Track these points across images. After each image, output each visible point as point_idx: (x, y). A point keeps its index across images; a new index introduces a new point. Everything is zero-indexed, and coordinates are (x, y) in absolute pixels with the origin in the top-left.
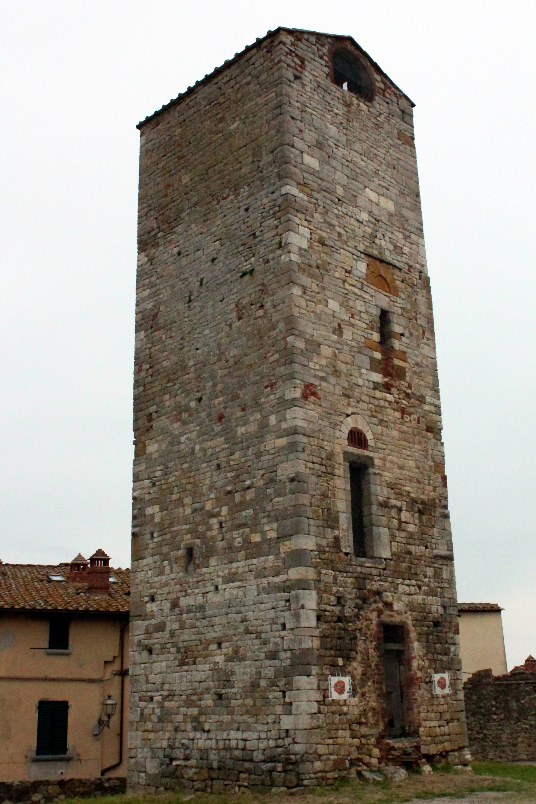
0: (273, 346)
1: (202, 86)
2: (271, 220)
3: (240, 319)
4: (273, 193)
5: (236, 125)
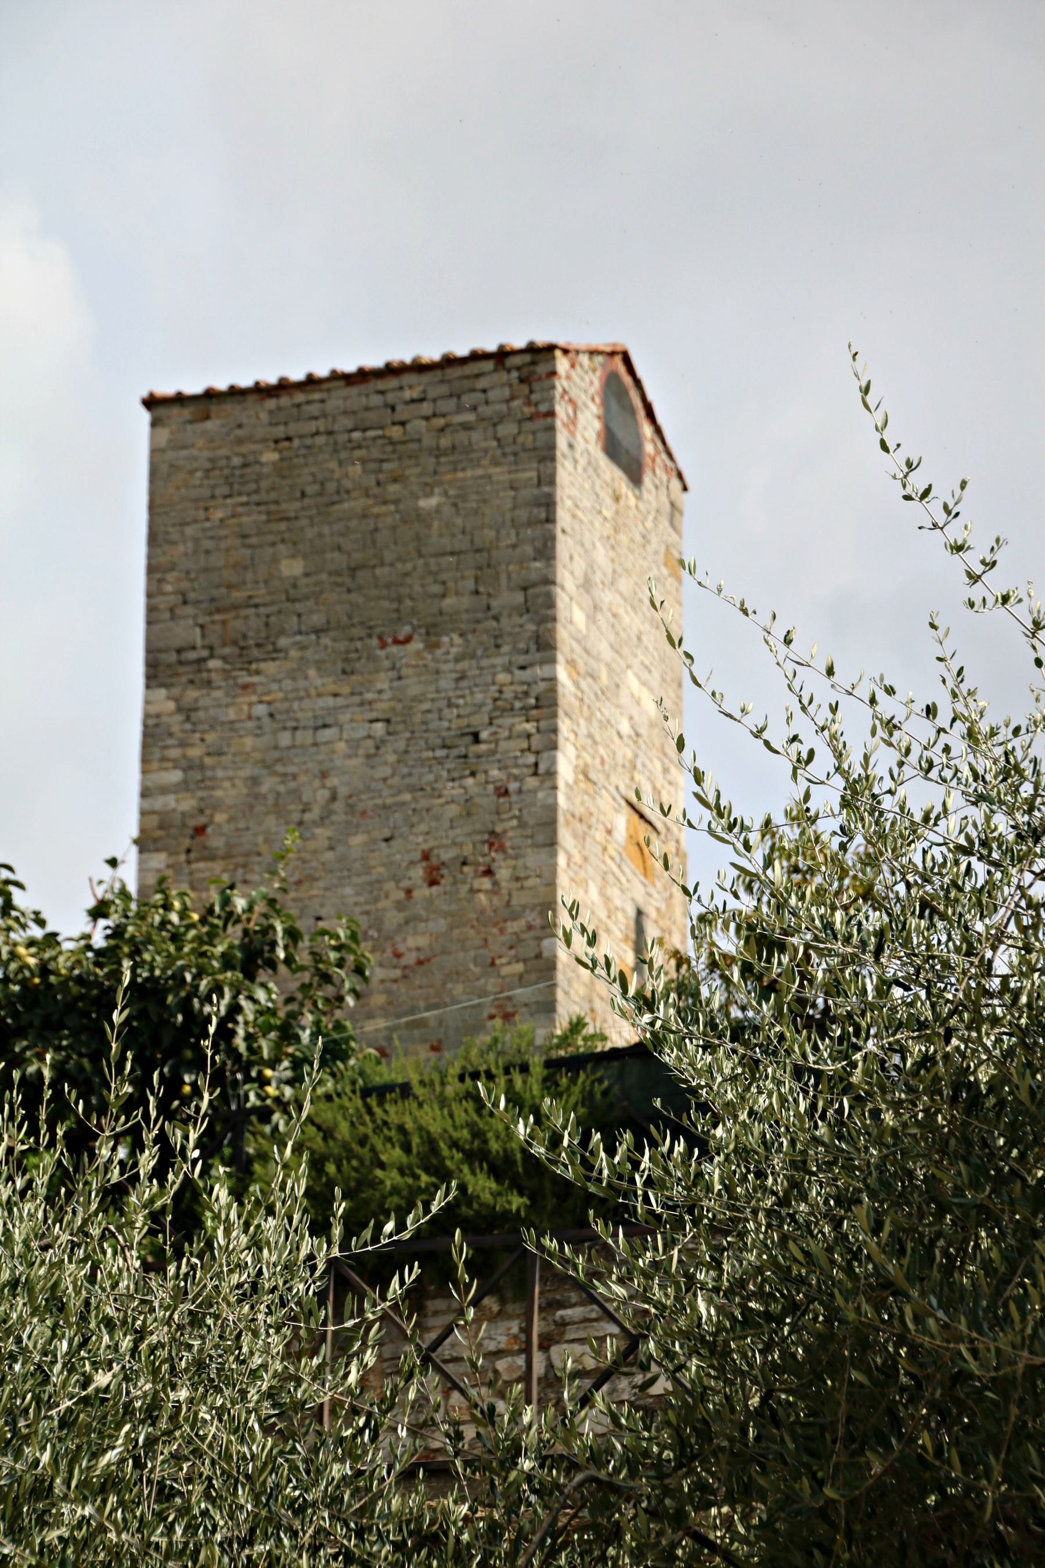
0: (511, 948)
1: (342, 383)
3: (433, 883)
4: (523, 668)
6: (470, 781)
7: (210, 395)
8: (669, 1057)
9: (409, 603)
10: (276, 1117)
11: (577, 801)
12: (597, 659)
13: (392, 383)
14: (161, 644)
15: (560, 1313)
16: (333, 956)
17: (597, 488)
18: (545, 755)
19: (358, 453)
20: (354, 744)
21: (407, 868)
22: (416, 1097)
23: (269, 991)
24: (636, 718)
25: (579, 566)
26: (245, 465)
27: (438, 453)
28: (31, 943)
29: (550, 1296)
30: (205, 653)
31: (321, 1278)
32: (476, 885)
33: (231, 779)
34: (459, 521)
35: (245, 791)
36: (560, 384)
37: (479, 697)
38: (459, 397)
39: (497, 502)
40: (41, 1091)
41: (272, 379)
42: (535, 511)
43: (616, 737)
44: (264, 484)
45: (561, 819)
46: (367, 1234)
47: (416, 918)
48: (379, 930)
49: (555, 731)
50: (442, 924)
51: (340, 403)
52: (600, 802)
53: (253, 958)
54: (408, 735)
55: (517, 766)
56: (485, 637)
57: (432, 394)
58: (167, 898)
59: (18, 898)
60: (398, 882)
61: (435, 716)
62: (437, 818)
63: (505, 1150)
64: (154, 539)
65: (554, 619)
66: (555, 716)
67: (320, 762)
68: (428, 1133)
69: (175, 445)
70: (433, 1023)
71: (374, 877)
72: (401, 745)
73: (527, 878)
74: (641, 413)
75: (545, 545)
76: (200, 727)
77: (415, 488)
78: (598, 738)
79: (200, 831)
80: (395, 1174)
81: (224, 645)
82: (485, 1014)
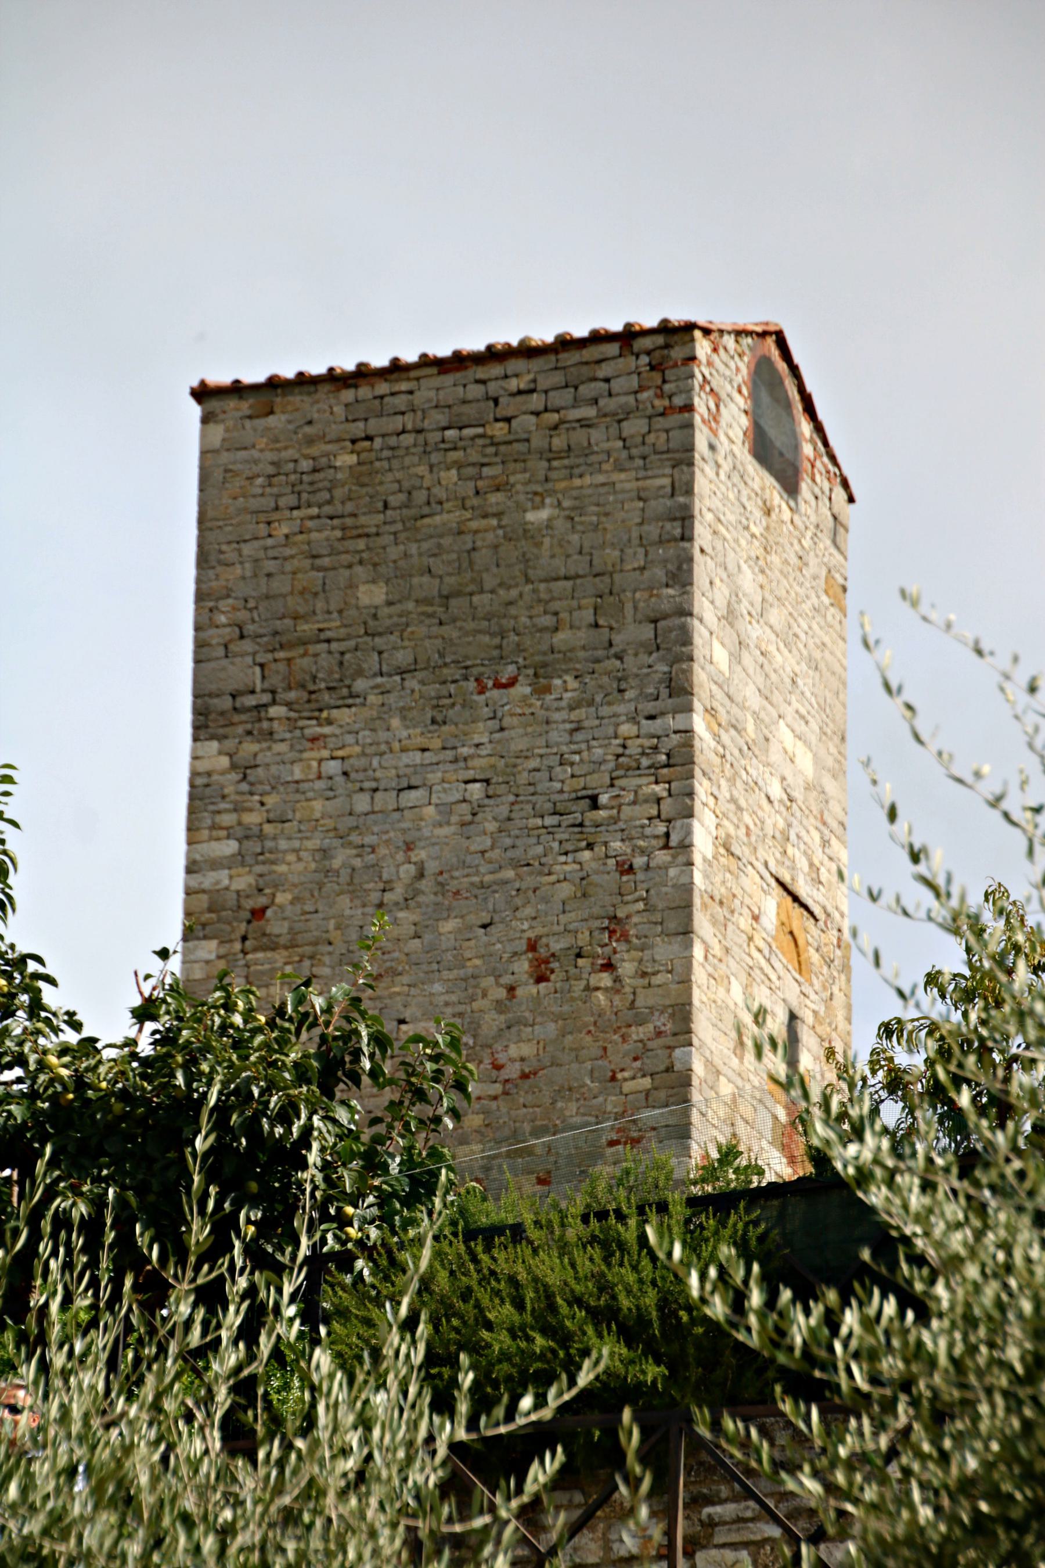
0: (636, 1059)
1: (434, 370)
2: (644, 780)
3: (540, 979)
4: (651, 717)
5: (544, 514)
6: (587, 854)
7: (274, 384)
8: (876, 1196)
9: (513, 638)
10: (360, 1263)
11: (718, 879)
12: (743, 708)
13: (496, 370)
14: (213, 687)
15: (708, 1510)
16: (430, 1066)
17: (744, 500)
18: (678, 823)
19: (453, 455)
20: (446, 810)
21: (510, 961)
22: (530, 1242)
23: (351, 1109)
24: (790, 779)
25: (722, 593)
26: (315, 470)
27: (550, 455)
28: (64, 1050)
29: (694, 1489)
30: (266, 698)
31: (444, 1464)
32: (593, 982)
33: (296, 851)
34: (575, 538)
35: (313, 866)
36: (699, 371)
37: (598, 752)
38: (576, 388)
39: (622, 515)
40: (102, 1233)
41: (349, 365)
42: (668, 526)
43: (764, 802)
44: (338, 493)
45: (697, 901)
46: (500, 1412)
47: (521, 1022)
48: (475, 1036)
49: (691, 794)
50: (552, 1029)
51: (432, 394)
52: (745, 881)
53: (332, 1070)
54: (511, 798)
55: (644, 837)
56: (605, 679)
57: (543, 383)
58: (228, 996)
59: (49, 995)
60: (498, 977)
61: (544, 775)
62: (546, 900)
63: (638, 1307)
64: (203, 559)
65: (691, 659)
66: (691, 776)
67: (404, 831)
68: (546, 1286)
69: (230, 446)
70: (538, 1151)
71: (470, 971)
72: (503, 811)
73: (655, 973)
74: (798, 406)
75: (679, 568)
76: (259, 788)
77: (522, 497)
78: (743, 803)
79: (258, 913)
80: (504, 1336)
81: (290, 688)
82: (604, 1141)
